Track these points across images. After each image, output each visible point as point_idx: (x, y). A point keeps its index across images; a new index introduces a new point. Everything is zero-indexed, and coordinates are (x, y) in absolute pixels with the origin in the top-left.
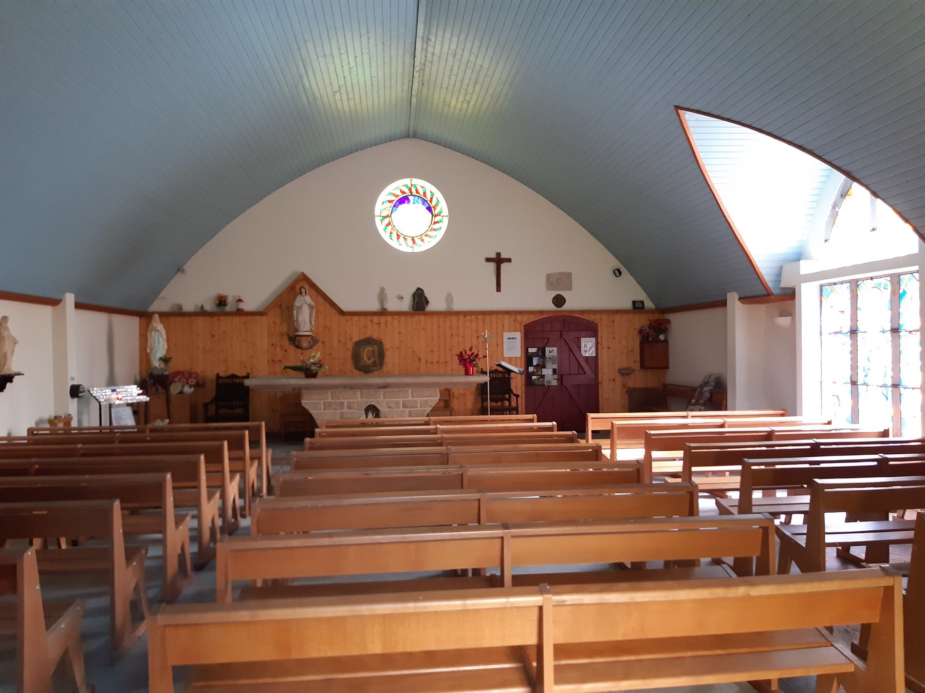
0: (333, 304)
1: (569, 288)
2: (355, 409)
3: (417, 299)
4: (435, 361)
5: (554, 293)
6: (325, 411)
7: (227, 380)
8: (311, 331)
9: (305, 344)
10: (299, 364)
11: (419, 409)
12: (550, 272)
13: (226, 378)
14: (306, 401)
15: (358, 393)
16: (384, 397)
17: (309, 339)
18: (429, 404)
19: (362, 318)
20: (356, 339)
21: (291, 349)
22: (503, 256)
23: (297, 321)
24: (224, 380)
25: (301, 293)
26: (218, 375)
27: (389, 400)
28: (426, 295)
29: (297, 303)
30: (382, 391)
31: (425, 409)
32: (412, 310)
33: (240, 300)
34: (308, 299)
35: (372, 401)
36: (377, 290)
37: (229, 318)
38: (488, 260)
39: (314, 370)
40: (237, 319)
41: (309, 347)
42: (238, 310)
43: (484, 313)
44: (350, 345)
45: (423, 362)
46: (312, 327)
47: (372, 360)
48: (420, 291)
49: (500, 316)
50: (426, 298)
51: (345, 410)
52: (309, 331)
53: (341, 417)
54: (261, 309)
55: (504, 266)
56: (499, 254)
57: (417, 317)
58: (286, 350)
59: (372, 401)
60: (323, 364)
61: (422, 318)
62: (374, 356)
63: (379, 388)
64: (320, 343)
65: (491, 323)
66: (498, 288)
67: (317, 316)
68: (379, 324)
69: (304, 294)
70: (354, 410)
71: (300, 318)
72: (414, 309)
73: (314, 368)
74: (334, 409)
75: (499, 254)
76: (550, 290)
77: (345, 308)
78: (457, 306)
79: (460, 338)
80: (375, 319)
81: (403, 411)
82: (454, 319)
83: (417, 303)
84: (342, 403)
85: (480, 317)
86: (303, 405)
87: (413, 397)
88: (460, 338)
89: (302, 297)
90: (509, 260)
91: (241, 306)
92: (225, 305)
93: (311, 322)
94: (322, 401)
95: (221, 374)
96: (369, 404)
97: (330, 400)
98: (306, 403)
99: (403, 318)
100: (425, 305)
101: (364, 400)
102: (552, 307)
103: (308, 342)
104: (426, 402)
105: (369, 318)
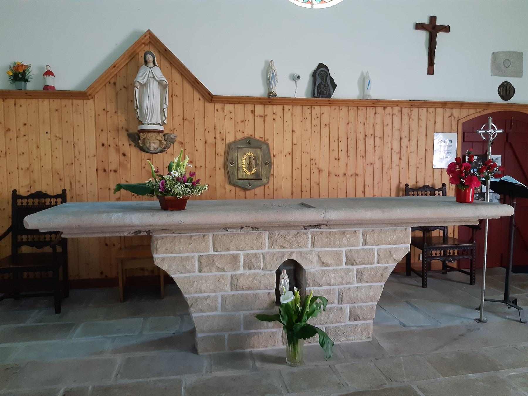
0: (196, 84)
1: (519, 74)
2: (259, 268)
3: (319, 81)
4: (341, 173)
5: (501, 80)
6: (200, 274)
7: (31, 201)
8: (163, 124)
9: (154, 145)
10: (149, 181)
11: (376, 265)
12: (496, 51)
13: (27, 197)
14: (161, 256)
15: (266, 236)
16: (313, 244)
17: (160, 137)
18: (394, 256)
19: (239, 107)
20: (230, 138)
21: (133, 152)
22: (439, 22)
23: (141, 107)
24: (25, 201)
25: (146, 62)
26: (14, 191)
27: (323, 249)
28: (332, 74)
29: (141, 78)
30: (310, 232)
31: (387, 265)
32: (309, 97)
33: (49, 73)
34: (157, 72)
35: (291, 253)
36: (261, 66)
37: (33, 102)
38: (419, 26)
39: (180, 194)
40: (45, 104)
41: (159, 149)
42: (46, 88)
43: (413, 104)
44: (221, 148)
45: (325, 174)
46: (164, 118)
47: (254, 170)
48: (323, 69)
49: (431, 110)
50: (332, 80)
51: (241, 271)
52: (159, 124)
53: (234, 286)
54: (83, 89)
55: (440, 37)
56: (433, 19)
57: (317, 108)
58: (124, 155)
59: (291, 253)
60: (198, 181)
61: (326, 109)
62: (256, 165)
63: (305, 228)
64: (176, 144)
65: (419, 119)
66: (430, 71)
67: (171, 101)
68: (264, 117)
69: (151, 65)
70: (257, 271)
71: (145, 104)
72: (316, 95)
73: (179, 189)
74: (220, 269)
75: (433, 19)
76: (495, 75)
77: (214, 92)
78: (375, 94)
79: (377, 139)
80: (259, 109)
81: (348, 270)
82: (370, 112)
83: (319, 86)
84: (235, 258)
85: (406, 111)
86: (158, 263)
87: (365, 243)
88: (377, 139)
89: (149, 69)
90: (446, 29)
91: (50, 81)
92: (26, 81)
93: (162, 111)
94: (196, 255)
95: (23, 191)
96: (285, 259)
97: (211, 252)
98: (163, 259)
99: (298, 110)
100: (332, 90)
101: (276, 250)
102: (497, 99)
103: (158, 142)
104: (390, 253)
105: (249, 107)
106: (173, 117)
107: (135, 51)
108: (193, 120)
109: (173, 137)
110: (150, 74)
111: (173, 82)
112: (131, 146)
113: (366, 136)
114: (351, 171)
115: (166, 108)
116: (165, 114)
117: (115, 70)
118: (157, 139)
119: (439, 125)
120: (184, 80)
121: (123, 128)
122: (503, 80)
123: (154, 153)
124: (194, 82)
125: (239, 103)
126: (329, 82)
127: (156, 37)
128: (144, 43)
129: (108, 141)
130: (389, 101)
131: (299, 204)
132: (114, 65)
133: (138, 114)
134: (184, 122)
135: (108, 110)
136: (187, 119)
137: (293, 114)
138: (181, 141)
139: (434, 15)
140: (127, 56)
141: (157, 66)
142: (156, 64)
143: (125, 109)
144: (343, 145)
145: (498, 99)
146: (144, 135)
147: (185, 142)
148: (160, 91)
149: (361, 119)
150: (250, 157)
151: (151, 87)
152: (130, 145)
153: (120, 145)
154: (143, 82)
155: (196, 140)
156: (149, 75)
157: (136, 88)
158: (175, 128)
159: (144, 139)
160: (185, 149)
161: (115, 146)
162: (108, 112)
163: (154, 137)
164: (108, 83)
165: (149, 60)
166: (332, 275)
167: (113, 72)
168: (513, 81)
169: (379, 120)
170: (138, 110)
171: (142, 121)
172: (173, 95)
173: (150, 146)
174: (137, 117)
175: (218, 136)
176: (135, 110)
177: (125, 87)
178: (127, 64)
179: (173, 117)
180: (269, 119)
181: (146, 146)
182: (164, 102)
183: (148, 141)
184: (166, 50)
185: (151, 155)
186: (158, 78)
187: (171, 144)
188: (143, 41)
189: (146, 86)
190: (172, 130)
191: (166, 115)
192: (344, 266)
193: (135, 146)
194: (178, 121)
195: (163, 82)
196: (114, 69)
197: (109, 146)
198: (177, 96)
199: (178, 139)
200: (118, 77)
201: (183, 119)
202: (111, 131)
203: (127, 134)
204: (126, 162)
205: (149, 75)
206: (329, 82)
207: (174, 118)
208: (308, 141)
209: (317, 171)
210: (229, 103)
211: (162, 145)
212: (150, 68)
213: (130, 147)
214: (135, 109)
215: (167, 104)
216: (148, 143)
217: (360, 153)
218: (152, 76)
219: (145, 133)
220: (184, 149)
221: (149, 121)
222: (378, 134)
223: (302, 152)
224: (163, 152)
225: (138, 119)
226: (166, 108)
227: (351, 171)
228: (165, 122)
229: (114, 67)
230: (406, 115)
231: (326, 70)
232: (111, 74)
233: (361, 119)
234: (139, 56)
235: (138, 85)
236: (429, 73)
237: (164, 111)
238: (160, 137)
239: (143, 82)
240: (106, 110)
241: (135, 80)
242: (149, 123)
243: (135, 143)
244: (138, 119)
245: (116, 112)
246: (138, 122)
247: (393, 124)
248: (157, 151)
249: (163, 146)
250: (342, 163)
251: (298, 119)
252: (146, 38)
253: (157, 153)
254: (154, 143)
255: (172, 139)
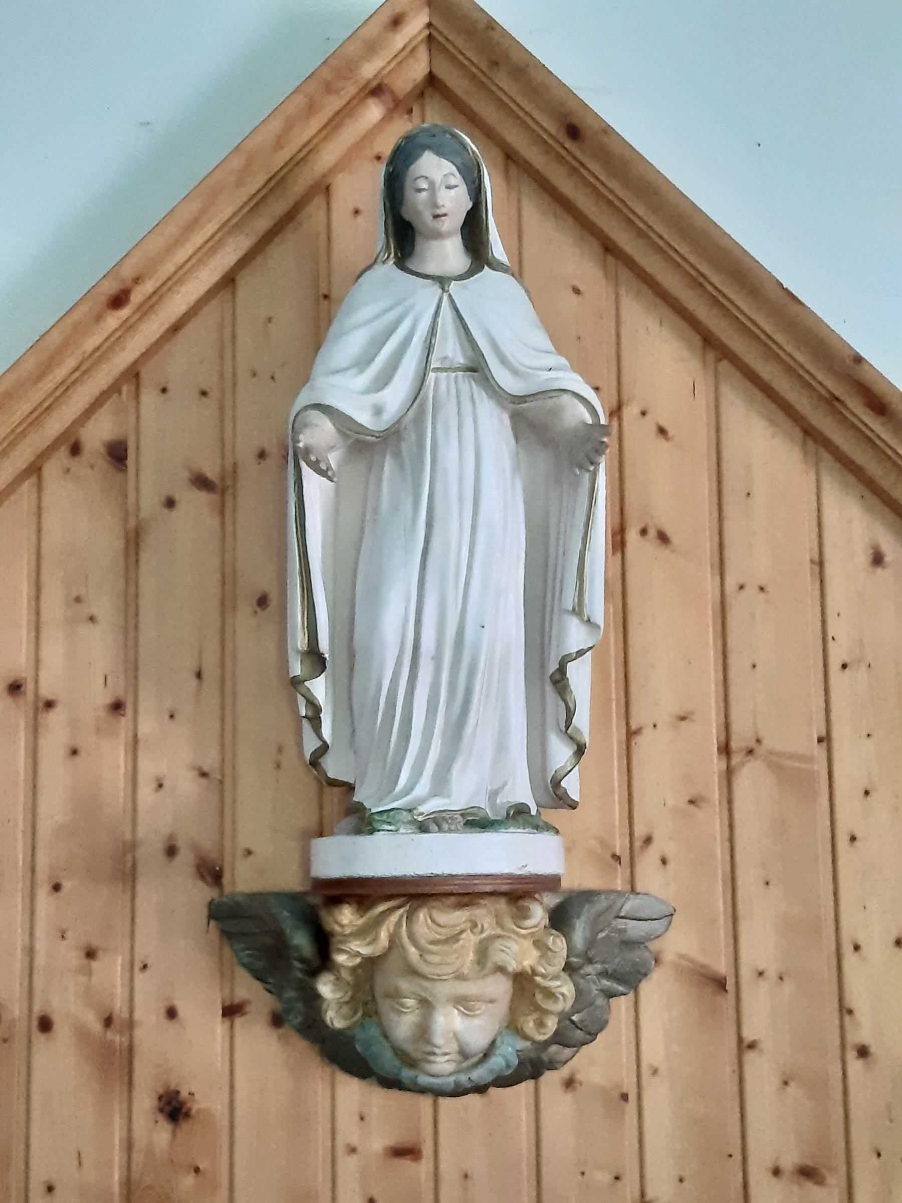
89: (428, 294)
106: (631, 734)
107: (297, 162)
108: (819, 752)
109: (635, 929)
110: (445, 339)
111: (630, 412)
112: (238, 1021)
115: (580, 653)
116: (570, 714)
117: (128, 327)
118: (501, 969)
120: (726, 390)
121: (171, 851)
123: (458, 1092)
124: (832, 402)
127: (492, 25)
128: (376, 90)
129: (38, 983)
132: (111, 288)
133: (315, 720)
134: (729, 774)
135: (46, 692)
136: (760, 751)
138: (702, 959)
140: (226, 209)
141: (496, 266)
142: (498, 249)
143: (199, 675)
146: (366, 932)
147: (746, 973)
148: (525, 490)
151: (450, 454)
152: (231, 1011)
153: (138, 1015)
154: (378, 411)
155: (848, 949)
156: (429, 349)
157: (305, 469)
158: (648, 840)
159: (370, 964)
160: (752, 1046)
161: (96, 1026)
162: (49, 705)
163: (470, 940)
164: (63, 454)
165: (435, 205)
167: (101, 354)
170: (319, 687)
171: (349, 788)
172: (632, 536)
173: (423, 1032)
174: (310, 744)
176: (296, 683)
177: (201, 482)
178: (229, 281)
179: (631, 734)
181: (380, 1025)
182: (569, 601)
183: (405, 985)
184: (574, 132)
185: (426, 1102)
186: (515, 372)
187: (610, 995)
188: (369, 70)
189: (397, 455)
190: (617, 858)
191: (582, 720)
193: (277, 1021)
195: (556, 412)
196: (113, 320)
197: (45, 1025)
198: (663, 538)
200: (149, 397)
201: (725, 750)
202: (67, 885)
203: (211, 904)
204: (189, 1180)
205: (429, 349)
207: (642, 743)
211: (538, 1008)
212: (442, 281)
213: (232, 1026)
214: (297, 669)
215: (599, 618)
216: (410, 1002)
218: (460, 360)
219: (382, 907)
220: (740, 1040)
221: (423, 788)
224: (535, 1075)
225: (315, 762)
226: (580, 653)
228: (572, 786)
229: (118, 301)
232: (83, 371)
234: (334, 206)
235: (332, 448)
237: (560, 681)
238: (528, 944)
239: (378, 411)
240: (29, 687)
241: (304, 399)
242: (427, 808)
243: (280, 997)
244: (315, 762)
245: (117, 707)
246: (314, 786)
247: (356, 675)
248: (480, 1074)
249: (540, 1024)
252: (400, 40)
253: (480, 1089)
254: (463, 1003)
255: (629, 944)
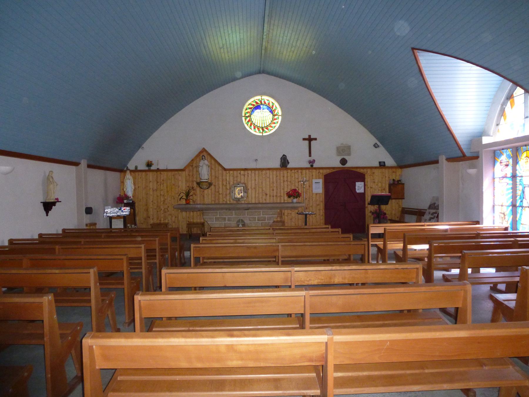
1: (349, 154)
38: (304, 139)
45: (268, 196)
50: (288, 161)
56: (310, 136)
68: (244, 175)
75: (310, 136)
83: (283, 163)
85: (300, 171)
90: (315, 139)
105: (239, 172)
113: (284, 181)
114: (279, 195)
119: (314, 177)
122: (342, 157)
125: (235, 170)
126: (286, 162)
130: (293, 168)
131: (452, 282)
137: (255, 174)
139: (310, 134)
144: (275, 185)
145: (341, 166)
149: (282, 175)
150: (239, 190)
166: (253, 224)
168: (346, 158)
169: (289, 175)
175: (228, 183)
180: (246, 176)
192: (257, 221)
194: (213, 178)
199: (214, 184)
206: (286, 162)
208: (261, 184)
209: (265, 195)
210: (232, 171)
217: (282, 188)
222: (289, 180)
223: (259, 187)
227: (279, 195)
230: (300, 173)
231: (285, 157)
233: (282, 175)
236: (309, 156)
250: (275, 191)
251: (257, 176)
